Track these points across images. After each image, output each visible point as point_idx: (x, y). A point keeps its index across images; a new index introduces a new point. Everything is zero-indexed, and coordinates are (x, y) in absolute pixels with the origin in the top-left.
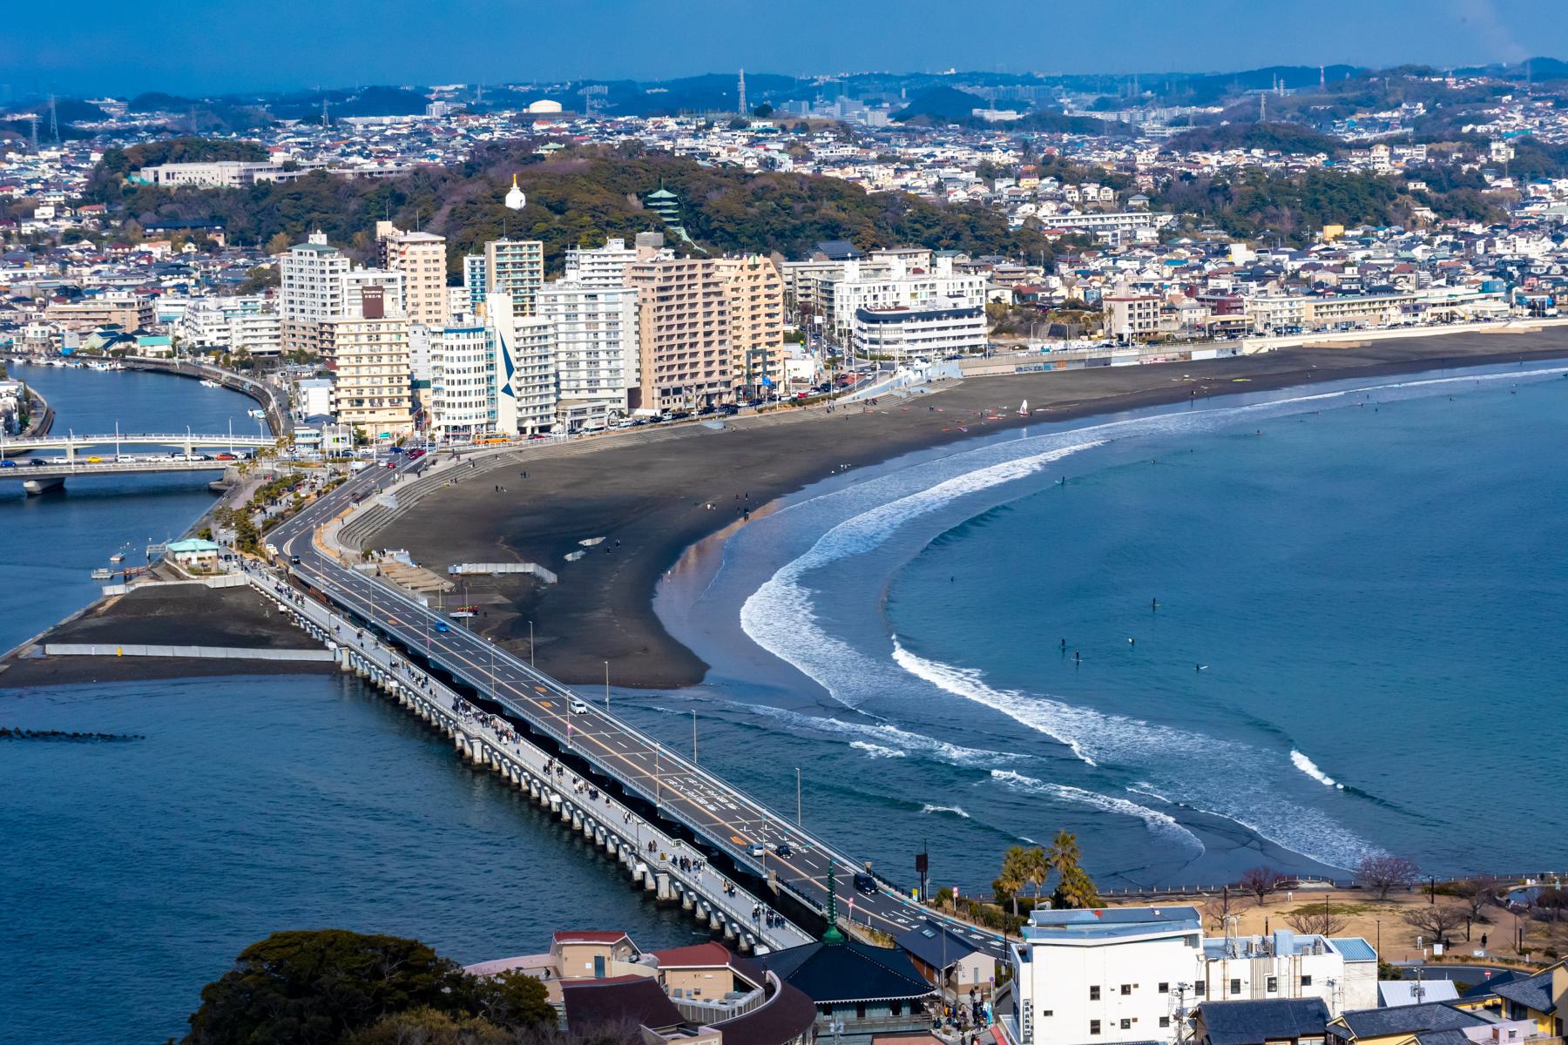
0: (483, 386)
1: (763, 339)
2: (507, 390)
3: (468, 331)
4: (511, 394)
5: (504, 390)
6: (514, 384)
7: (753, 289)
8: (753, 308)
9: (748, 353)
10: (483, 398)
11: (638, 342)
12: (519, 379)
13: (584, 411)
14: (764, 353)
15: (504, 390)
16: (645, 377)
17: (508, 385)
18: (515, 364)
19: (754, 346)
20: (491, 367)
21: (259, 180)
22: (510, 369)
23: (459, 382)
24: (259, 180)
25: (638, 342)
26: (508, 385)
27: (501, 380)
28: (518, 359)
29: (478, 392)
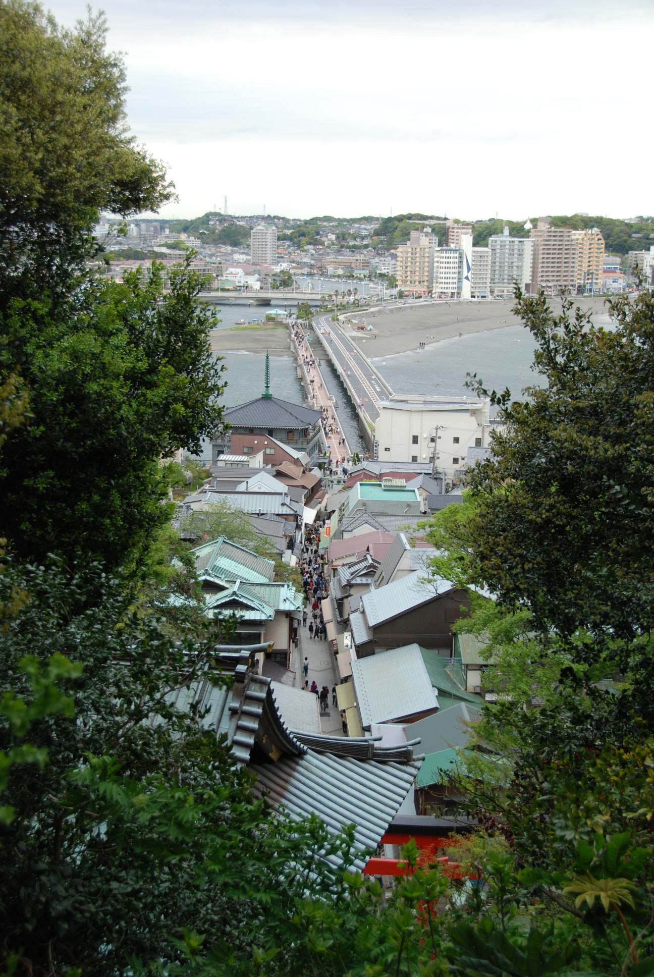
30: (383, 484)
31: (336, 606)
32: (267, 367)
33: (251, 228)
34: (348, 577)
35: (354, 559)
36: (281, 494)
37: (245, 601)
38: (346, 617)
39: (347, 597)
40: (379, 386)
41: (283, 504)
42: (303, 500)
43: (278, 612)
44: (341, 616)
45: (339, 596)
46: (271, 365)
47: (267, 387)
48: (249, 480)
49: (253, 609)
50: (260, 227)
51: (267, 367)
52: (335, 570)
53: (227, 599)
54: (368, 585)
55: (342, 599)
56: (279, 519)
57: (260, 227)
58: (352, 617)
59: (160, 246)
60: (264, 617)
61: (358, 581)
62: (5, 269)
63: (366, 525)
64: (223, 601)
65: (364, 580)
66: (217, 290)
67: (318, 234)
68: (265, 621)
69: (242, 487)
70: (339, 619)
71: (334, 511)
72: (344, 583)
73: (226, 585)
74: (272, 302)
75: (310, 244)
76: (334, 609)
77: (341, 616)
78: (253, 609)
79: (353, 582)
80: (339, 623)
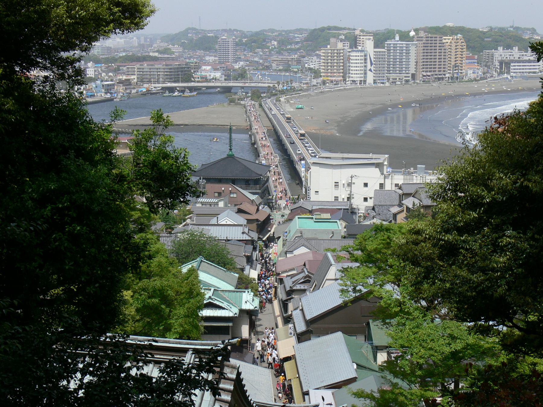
0: (363, 58)
1: (459, 62)
2: (370, 70)
3: (360, 51)
4: (372, 72)
5: (369, 70)
6: (372, 69)
7: (456, 46)
8: (456, 58)
9: (453, 66)
10: (362, 68)
11: (416, 68)
12: (374, 67)
13: (396, 79)
14: (458, 66)
15: (369, 70)
16: (418, 70)
17: (371, 69)
18: (374, 63)
19: (456, 64)
20: (365, 63)
21: (395, 311)
22: (371, 64)
23: (355, 56)
24: (395, 311)
25: (416, 68)
26: (371, 69)
27: (369, 67)
28: (374, 61)
29: (361, 60)
37: (218, 303)
41: (243, 233)
43: (242, 311)
48: (218, 216)
50: (224, 37)
59: (154, 52)
60: (231, 315)
61: (298, 287)
68: (232, 317)
71: (279, 237)
78: (224, 309)
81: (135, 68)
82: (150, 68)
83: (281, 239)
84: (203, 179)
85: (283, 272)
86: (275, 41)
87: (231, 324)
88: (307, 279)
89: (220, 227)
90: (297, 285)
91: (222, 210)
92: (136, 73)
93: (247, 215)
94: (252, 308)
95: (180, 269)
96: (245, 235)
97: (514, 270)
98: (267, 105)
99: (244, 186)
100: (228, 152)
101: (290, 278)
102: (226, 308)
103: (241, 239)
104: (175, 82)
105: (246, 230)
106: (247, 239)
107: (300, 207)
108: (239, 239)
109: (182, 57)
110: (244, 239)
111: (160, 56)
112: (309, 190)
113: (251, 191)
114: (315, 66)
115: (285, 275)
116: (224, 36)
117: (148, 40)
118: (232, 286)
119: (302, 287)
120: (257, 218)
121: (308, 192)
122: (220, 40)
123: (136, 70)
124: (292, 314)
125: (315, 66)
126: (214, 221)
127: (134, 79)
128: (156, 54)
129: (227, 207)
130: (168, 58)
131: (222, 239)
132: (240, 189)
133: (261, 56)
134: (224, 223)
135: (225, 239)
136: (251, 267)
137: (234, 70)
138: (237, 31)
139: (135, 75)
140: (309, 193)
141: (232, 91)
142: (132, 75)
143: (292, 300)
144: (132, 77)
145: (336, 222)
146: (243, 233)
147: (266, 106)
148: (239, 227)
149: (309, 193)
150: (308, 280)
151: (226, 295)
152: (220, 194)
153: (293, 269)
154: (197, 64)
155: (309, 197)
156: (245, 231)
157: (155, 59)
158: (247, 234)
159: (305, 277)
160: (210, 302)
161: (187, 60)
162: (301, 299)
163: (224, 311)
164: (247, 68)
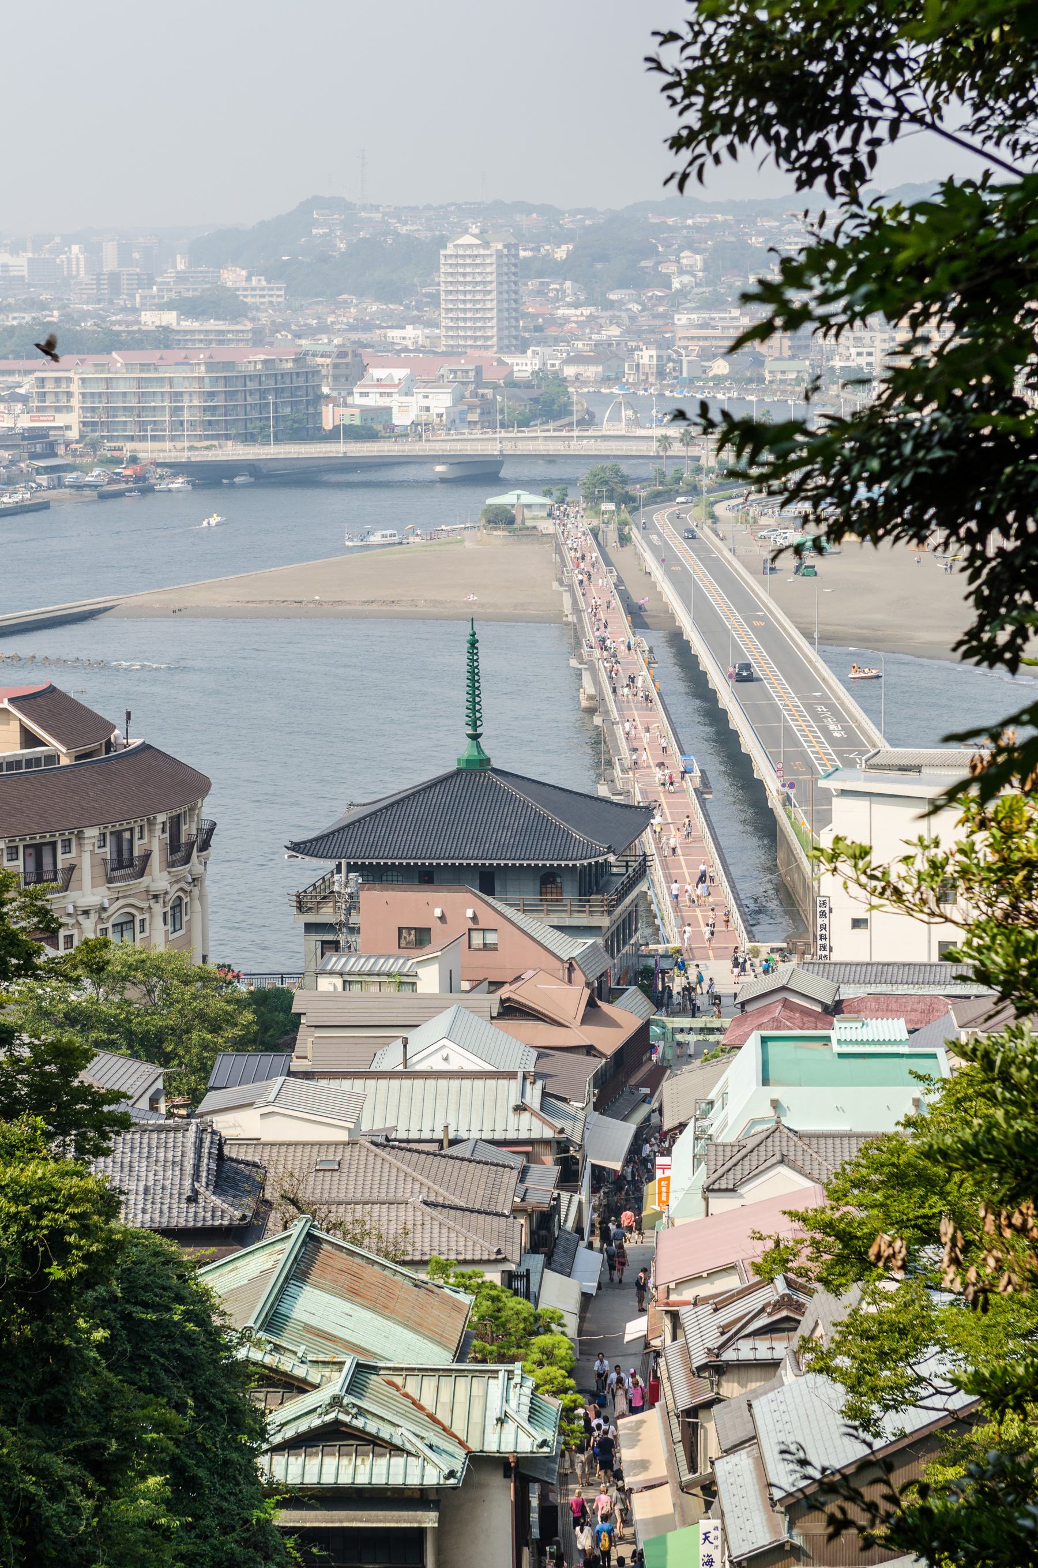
30: (834, 1035)
31: (678, 1435)
32: (474, 675)
33: (442, 242)
34: (714, 1340)
35: (731, 1283)
36: (511, 1075)
37: (372, 1427)
38: (704, 1469)
39: (708, 1405)
40: (839, 719)
41: (520, 1109)
42: (588, 1092)
43: (478, 1461)
44: (693, 1468)
45: (685, 1401)
46: (485, 664)
47: (475, 737)
48: (410, 1034)
49: (396, 1450)
50: (467, 240)
51: (474, 675)
52: (675, 1316)
53: (315, 1422)
54: (774, 1365)
55: (692, 1412)
56: (503, 1155)
57: (467, 240)
58: (722, 1469)
59: (162, 307)
60: (432, 1478)
61: (744, 1350)
62: (843, 456)
63: (782, 1169)
64: (303, 1426)
65: (763, 1349)
66: (333, 436)
67: (650, 251)
68: (439, 1489)
69: (390, 1059)
70: (687, 1477)
71: (682, 1127)
72: (700, 1359)
73: (314, 1377)
74: (505, 473)
75: (622, 284)
76: (671, 1442)
77: (693, 1468)
78: (396, 1450)
79: (729, 1355)
80: (684, 1488)
81: (69, 380)
82: (139, 380)
83: (688, 1133)
84: (351, 868)
85: (681, 1283)
86: (697, 252)
87: (429, 1520)
88: (784, 1313)
89: (419, 1083)
90: (741, 1344)
91: (431, 1008)
92: (75, 402)
93: (531, 1023)
94: (526, 1445)
95: (912, 1516)
96: (526, 1115)
97: (861, 54)
98: (654, 538)
99: (531, 897)
100: (465, 749)
101: (709, 1308)
102: (408, 1447)
103: (511, 1135)
104: (248, 438)
105: (534, 1096)
106: (535, 1135)
107: (784, 988)
108: (499, 1135)
109: (286, 326)
110: (524, 1135)
111: (187, 324)
112: (823, 914)
113: (556, 919)
114: (870, 359)
115: (688, 1294)
116: (466, 231)
117: (136, 255)
118: (445, 1347)
119: (763, 1349)
120: (589, 1043)
121: (820, 921)
122: (448, 252)
123: (75, 388)
124: (713, 1473)
125: (870, 359)
126: (390, 1059)
127: (68, 428)
128: (170, 318)
129: (453, 995)
130: (222, 332)
131: (427, 1135)
132: (510, 912)
133: (633, 318)
134: (436, 1064)
135: (439, 1135)
136: (548, 1264)
137: (513, 384)
138: (527, 209)
139: (69, 409)
140: (823, 927)
141: (501, 475)
142: (58, 409)
143: (715, 1408)
144: (61, 420)
145: (934, 1056)
146: (520, 1109)
147: (650, 544)
148: (503, 1083)
149: (823, 927)
150: (787, 1319)
151: (426, 1392)
152: (422, 936)
153: (729, 1269)
154: (349, 359)
155: (824, 947)
156: (527, 1101)
157: (164, 339)
158: (534, 1113)
159: (778, 1305)
160: (337, 1422)
161: (305, 343)
162: (754, 1404)
163: (398, 1461)
164: (569, 371)
